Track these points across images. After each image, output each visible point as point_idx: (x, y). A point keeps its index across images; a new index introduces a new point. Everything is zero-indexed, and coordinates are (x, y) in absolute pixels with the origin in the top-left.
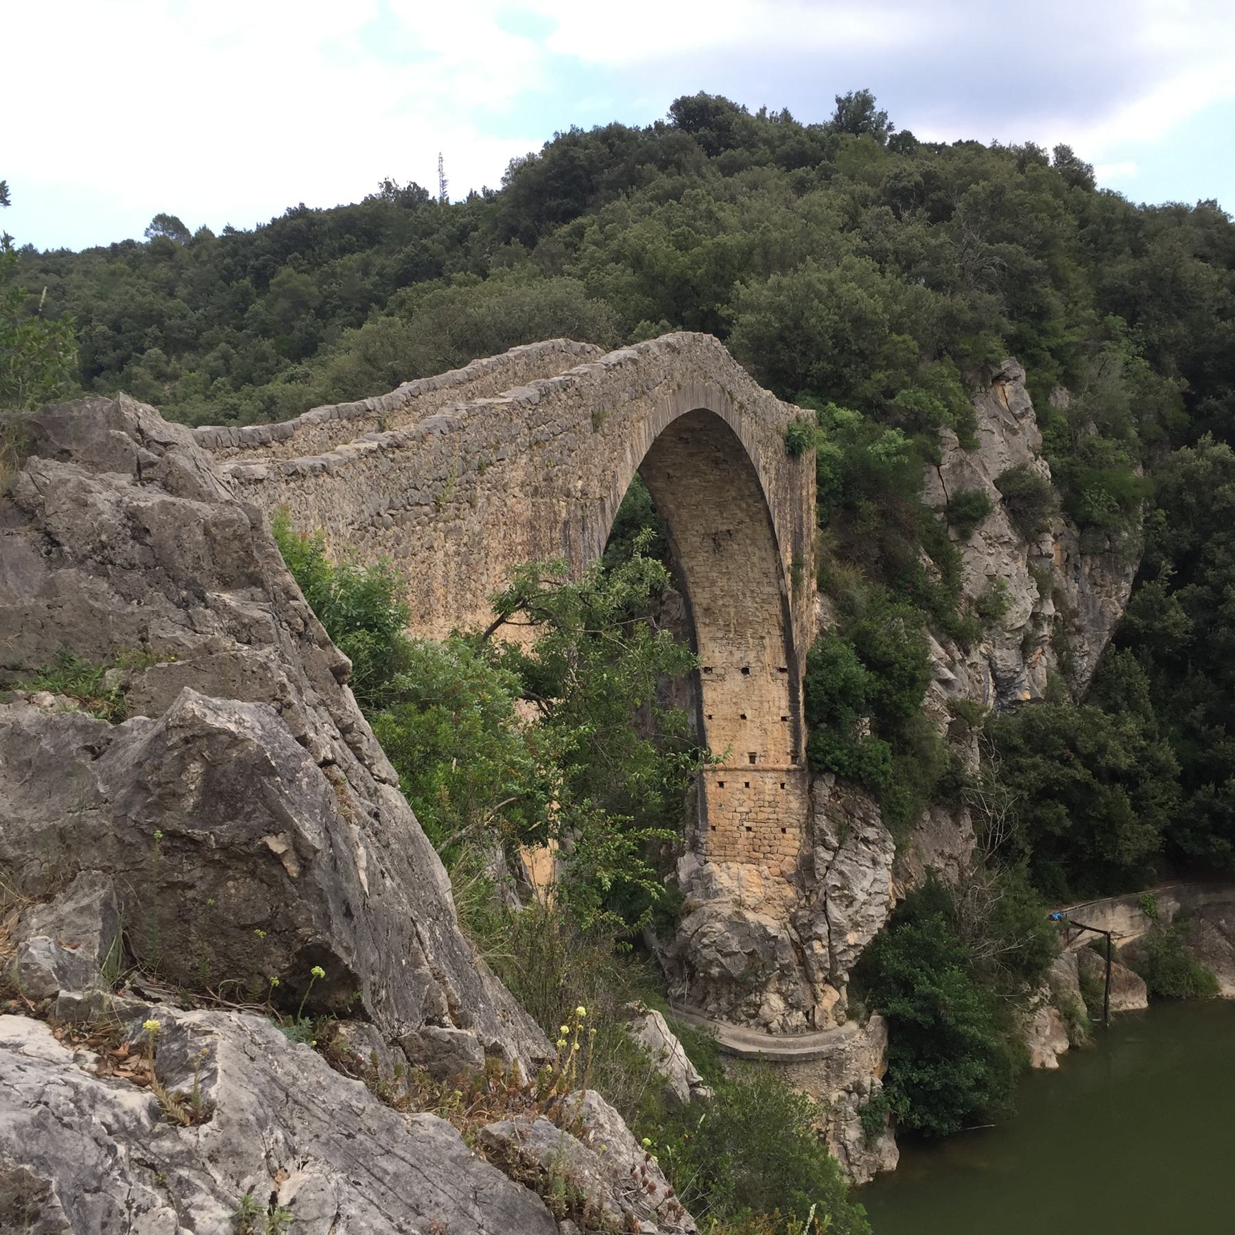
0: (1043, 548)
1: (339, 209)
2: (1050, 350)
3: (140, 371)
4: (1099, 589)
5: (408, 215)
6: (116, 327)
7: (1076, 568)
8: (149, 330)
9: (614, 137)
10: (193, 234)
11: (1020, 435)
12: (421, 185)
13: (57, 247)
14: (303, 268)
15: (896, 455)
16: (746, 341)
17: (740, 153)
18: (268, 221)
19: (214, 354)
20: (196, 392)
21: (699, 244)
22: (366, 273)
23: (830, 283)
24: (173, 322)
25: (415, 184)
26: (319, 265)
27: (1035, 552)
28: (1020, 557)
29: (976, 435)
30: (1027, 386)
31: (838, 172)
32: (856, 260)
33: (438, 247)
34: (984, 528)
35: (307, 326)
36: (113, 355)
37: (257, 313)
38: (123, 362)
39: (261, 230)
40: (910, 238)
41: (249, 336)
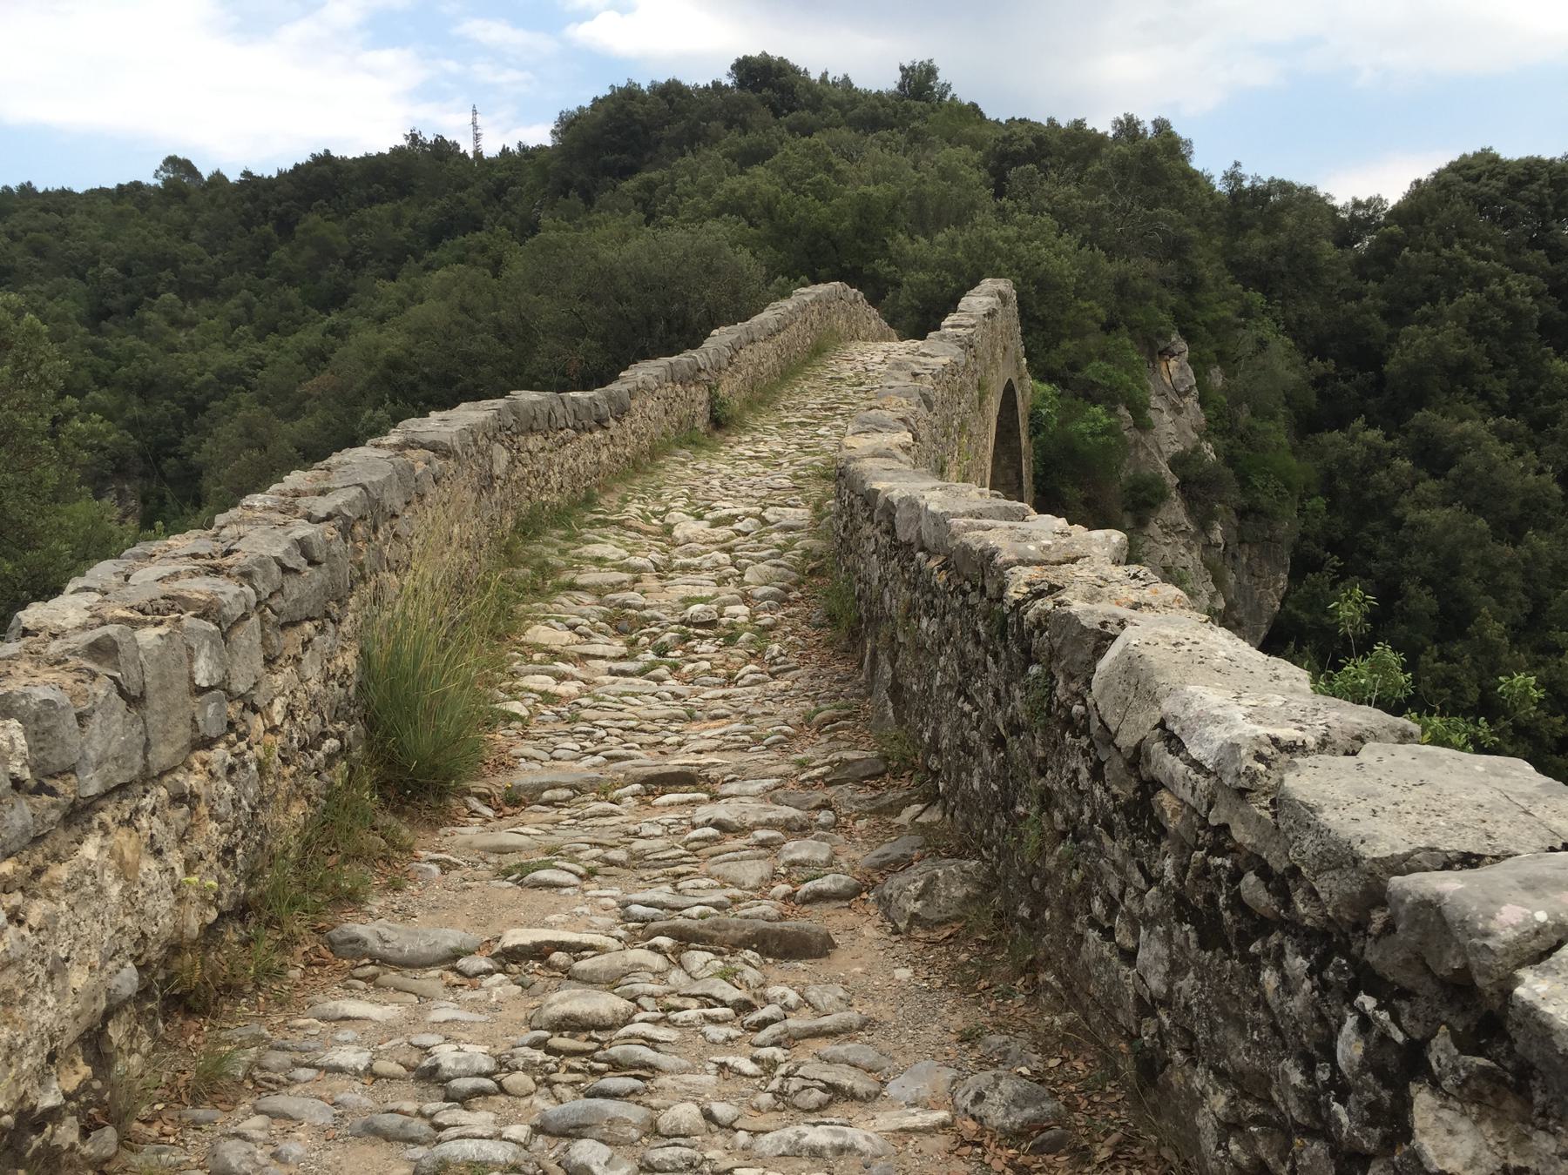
0: (1212, 537)
1: (367, 159)
2: (1206, 324)
4: (1256, 580)
6: (126, 269)
7: (1234, 557)
8: (163, 274)
10: (206, 178)
11: (1184, 414)
13: (58, 187)
14: (330, 216)
16: (916, 302)
17: (805, 114)
18: (289, 166)
19: (235, 301)
20: (216, 340)
24: (192, 266)
26: (348, 216)
28: (1195, 548)
30: (1190, 361)
34: (1159, 515)
36: (121, 298)
38: (132, 308)
39: (281, 174)
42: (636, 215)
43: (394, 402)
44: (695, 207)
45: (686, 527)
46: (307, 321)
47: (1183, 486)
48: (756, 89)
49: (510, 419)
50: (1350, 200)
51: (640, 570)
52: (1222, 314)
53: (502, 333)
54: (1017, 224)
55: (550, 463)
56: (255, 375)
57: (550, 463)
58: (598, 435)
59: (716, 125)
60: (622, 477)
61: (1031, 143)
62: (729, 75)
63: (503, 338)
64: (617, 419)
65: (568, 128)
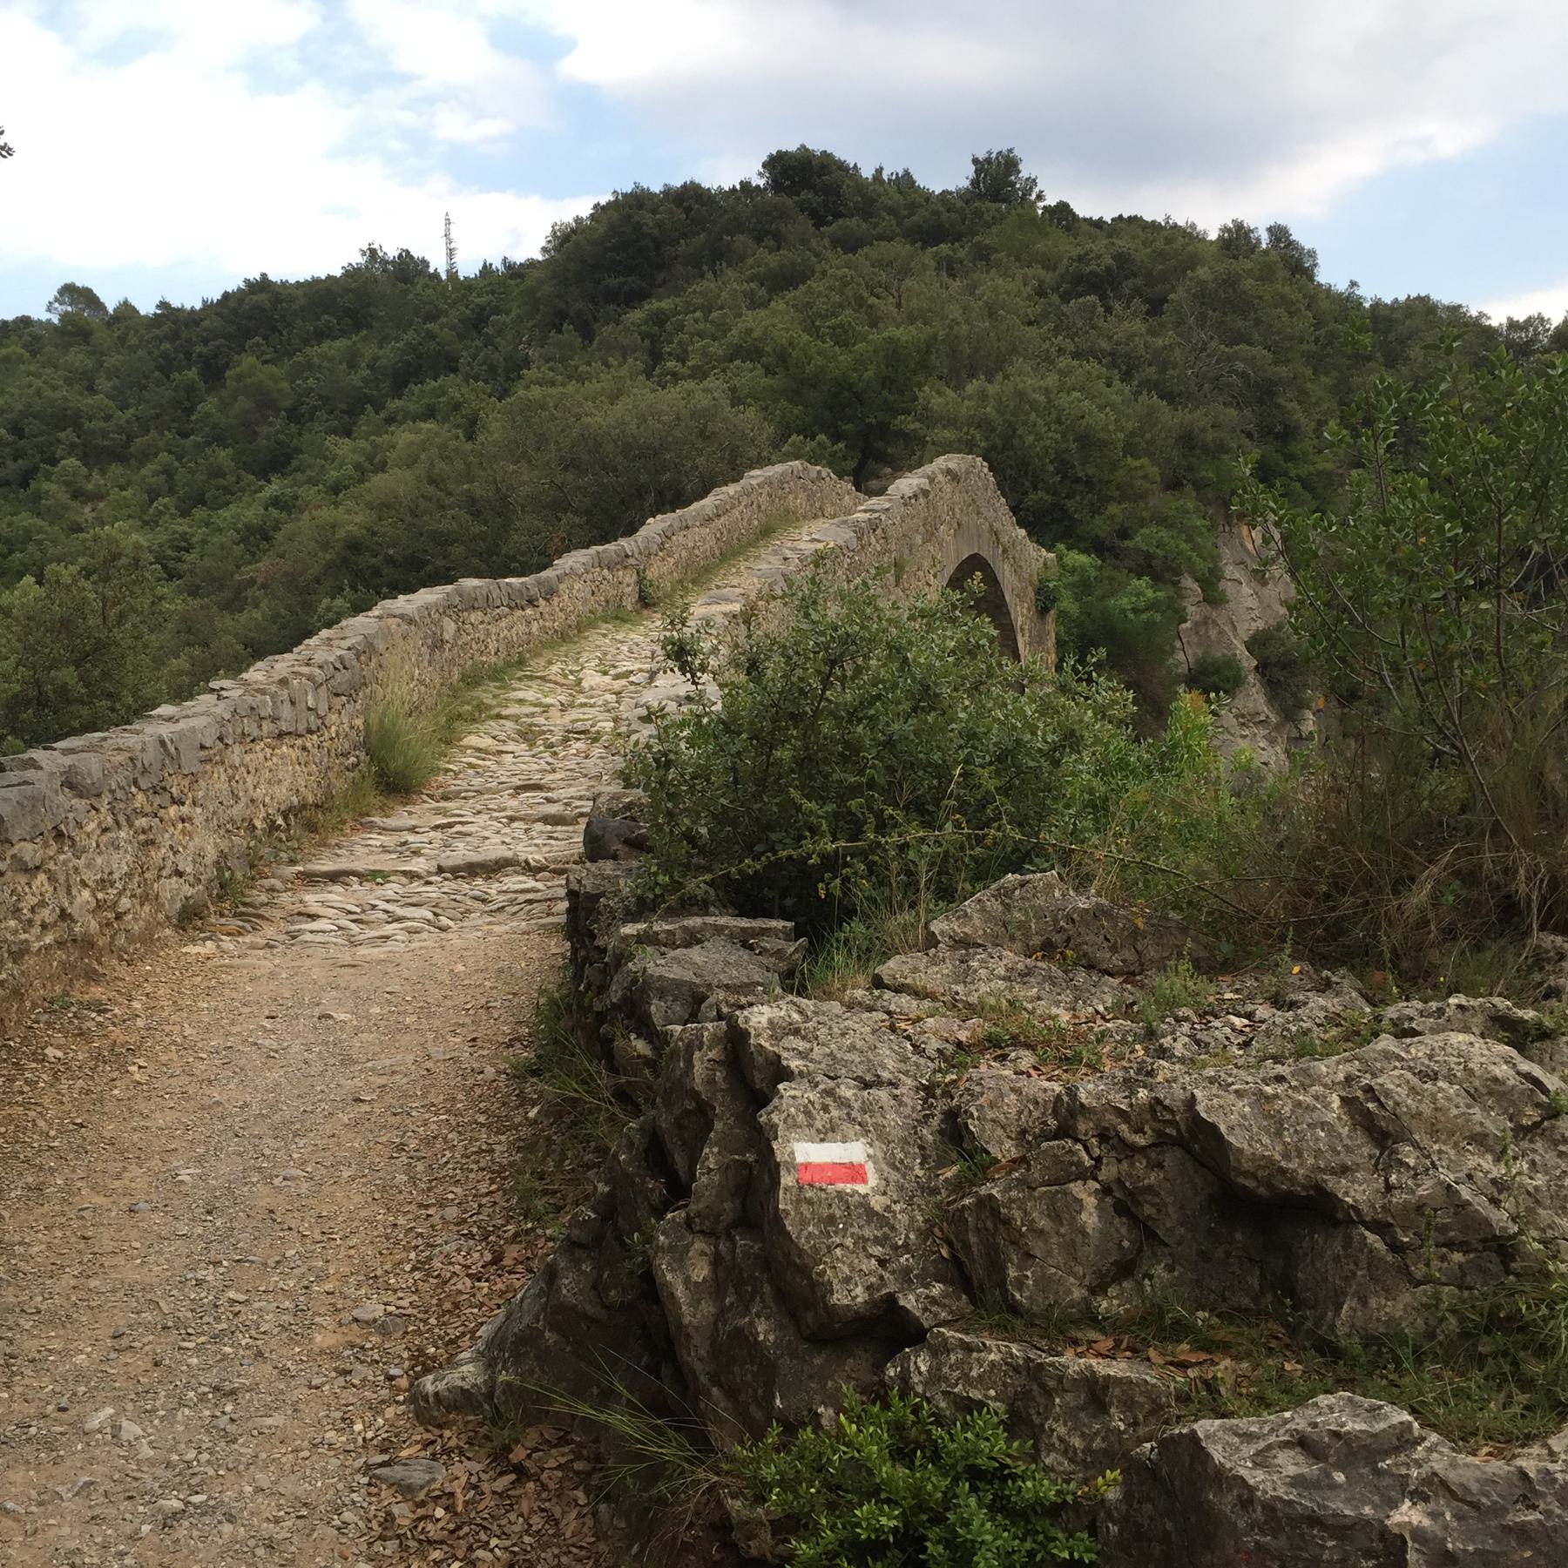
1: (316, 282)
2: (1300, 479)
3: (51, 488)
5: (405, 292)
8: (62, 435)
9: (690, 198)
10: (111, 311)
12: (416, 254)
14: (267, 357)
15: (1144, 611)
17: (853, 223)
21: (865, 339)
22: (352, 365)
23: (1047, 391)
24: (98, 424)
25: (408, 252)
26: (291, 356)
27: (1294, 734)
29: (1222, 585)
31: (997, 251)
32: (1076, 363)
33: (446, 334)
35: (277, 432)
36: (11, 465)
37: (208, 415)
38: (25, 480)
39: (208, 307)
40: (1130, 337)
41: (197, 444)
42: (635, 363)
43: (354, 588)
44: (704, 352)
45: (592, 679)
46: (242, 490)
47: (1262, 668)
48: (792, 191)
49: (457, 600)
50: (1504, 321)
51: (548, 706)
52: (1321, 466)
53: (474, 507)
54: (1060, 372)
55: (488, 634)
56: (179, 560)
57: (488, 634)
58: (529, 611)
59: (741, 239)
60: (551, 645)
61: (1111, 262)
62: (760, 174)
63: (476, 514)
64: (547, 600)
65: (561, 245)
